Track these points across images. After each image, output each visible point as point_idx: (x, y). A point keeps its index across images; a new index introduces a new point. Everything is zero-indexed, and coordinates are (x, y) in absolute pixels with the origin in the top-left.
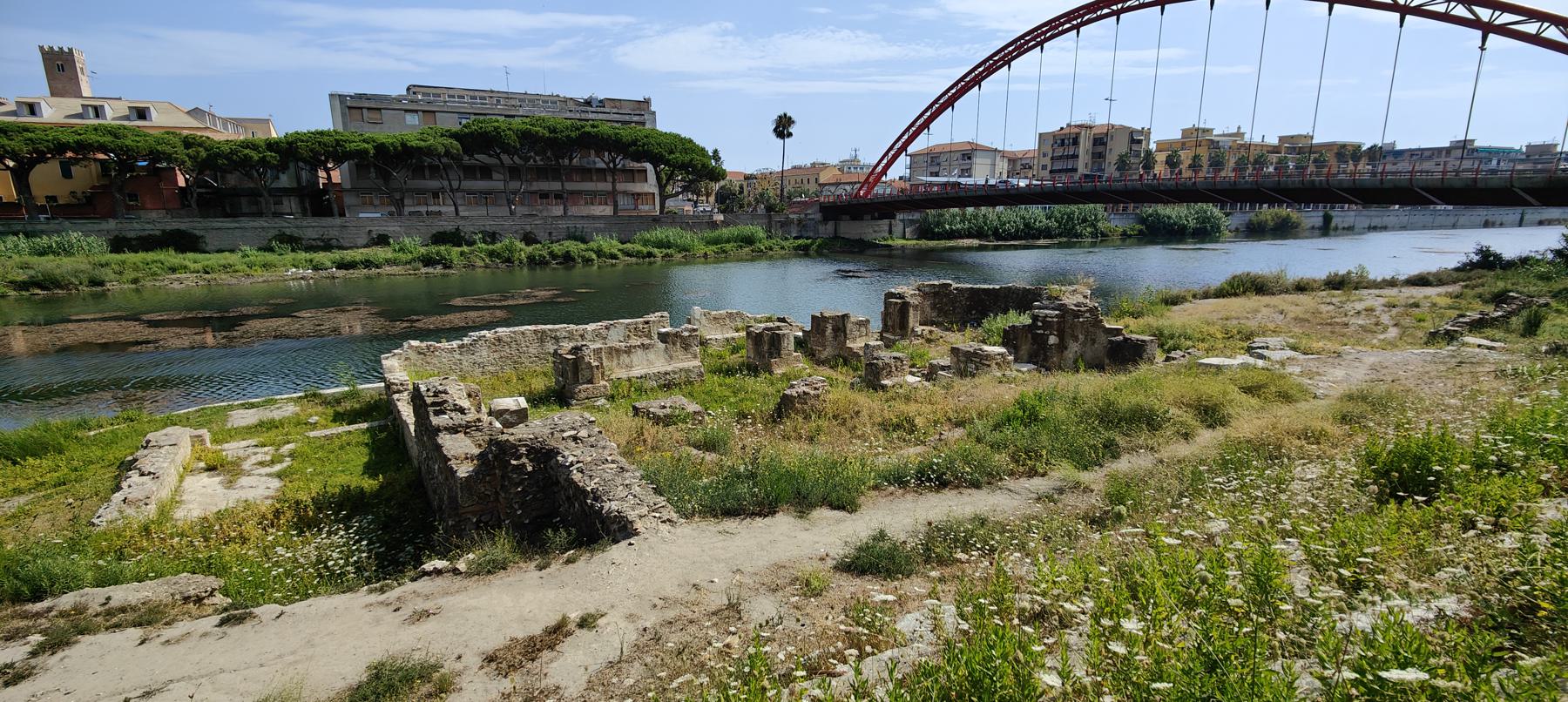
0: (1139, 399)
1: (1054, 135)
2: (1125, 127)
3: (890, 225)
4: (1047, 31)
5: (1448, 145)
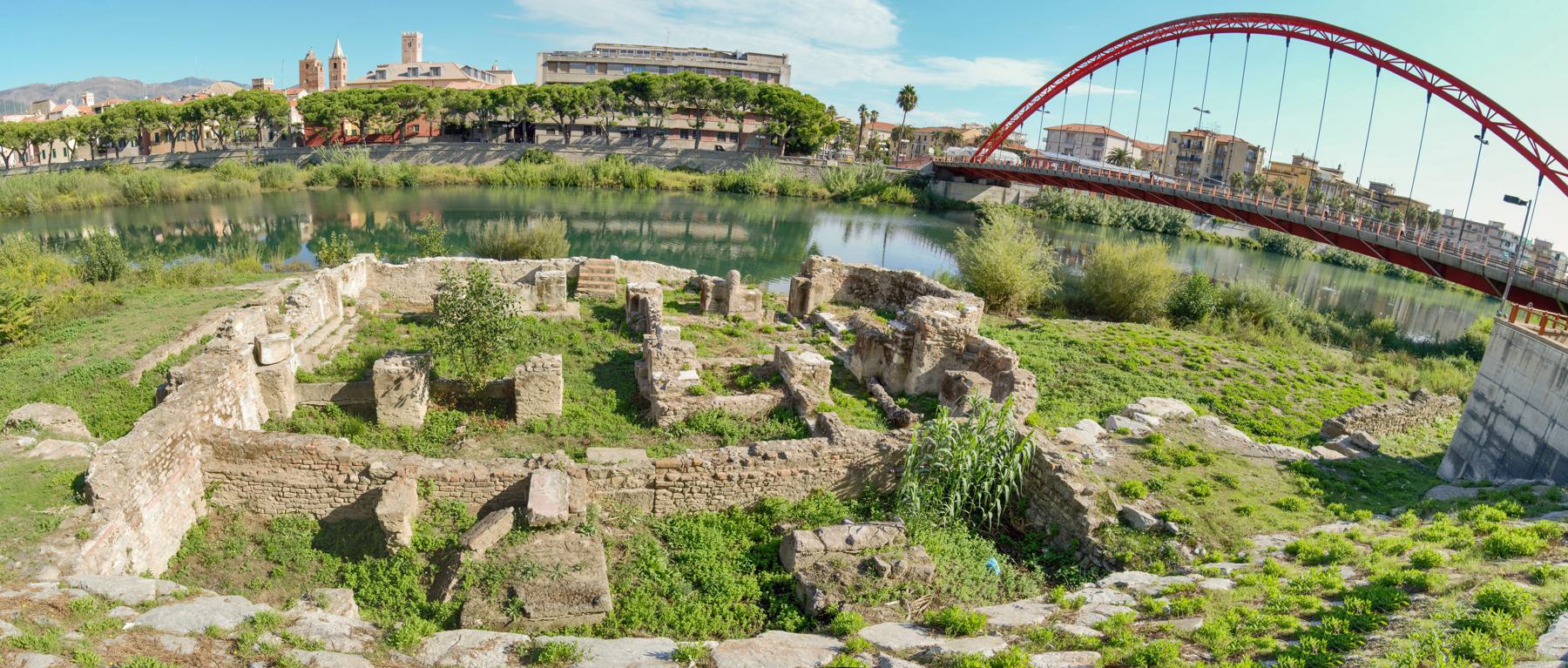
1: (1183, 135)
2: (1243, 142)
3: (1004, 193)
4: (1184, 27)
5: (1487, 223)
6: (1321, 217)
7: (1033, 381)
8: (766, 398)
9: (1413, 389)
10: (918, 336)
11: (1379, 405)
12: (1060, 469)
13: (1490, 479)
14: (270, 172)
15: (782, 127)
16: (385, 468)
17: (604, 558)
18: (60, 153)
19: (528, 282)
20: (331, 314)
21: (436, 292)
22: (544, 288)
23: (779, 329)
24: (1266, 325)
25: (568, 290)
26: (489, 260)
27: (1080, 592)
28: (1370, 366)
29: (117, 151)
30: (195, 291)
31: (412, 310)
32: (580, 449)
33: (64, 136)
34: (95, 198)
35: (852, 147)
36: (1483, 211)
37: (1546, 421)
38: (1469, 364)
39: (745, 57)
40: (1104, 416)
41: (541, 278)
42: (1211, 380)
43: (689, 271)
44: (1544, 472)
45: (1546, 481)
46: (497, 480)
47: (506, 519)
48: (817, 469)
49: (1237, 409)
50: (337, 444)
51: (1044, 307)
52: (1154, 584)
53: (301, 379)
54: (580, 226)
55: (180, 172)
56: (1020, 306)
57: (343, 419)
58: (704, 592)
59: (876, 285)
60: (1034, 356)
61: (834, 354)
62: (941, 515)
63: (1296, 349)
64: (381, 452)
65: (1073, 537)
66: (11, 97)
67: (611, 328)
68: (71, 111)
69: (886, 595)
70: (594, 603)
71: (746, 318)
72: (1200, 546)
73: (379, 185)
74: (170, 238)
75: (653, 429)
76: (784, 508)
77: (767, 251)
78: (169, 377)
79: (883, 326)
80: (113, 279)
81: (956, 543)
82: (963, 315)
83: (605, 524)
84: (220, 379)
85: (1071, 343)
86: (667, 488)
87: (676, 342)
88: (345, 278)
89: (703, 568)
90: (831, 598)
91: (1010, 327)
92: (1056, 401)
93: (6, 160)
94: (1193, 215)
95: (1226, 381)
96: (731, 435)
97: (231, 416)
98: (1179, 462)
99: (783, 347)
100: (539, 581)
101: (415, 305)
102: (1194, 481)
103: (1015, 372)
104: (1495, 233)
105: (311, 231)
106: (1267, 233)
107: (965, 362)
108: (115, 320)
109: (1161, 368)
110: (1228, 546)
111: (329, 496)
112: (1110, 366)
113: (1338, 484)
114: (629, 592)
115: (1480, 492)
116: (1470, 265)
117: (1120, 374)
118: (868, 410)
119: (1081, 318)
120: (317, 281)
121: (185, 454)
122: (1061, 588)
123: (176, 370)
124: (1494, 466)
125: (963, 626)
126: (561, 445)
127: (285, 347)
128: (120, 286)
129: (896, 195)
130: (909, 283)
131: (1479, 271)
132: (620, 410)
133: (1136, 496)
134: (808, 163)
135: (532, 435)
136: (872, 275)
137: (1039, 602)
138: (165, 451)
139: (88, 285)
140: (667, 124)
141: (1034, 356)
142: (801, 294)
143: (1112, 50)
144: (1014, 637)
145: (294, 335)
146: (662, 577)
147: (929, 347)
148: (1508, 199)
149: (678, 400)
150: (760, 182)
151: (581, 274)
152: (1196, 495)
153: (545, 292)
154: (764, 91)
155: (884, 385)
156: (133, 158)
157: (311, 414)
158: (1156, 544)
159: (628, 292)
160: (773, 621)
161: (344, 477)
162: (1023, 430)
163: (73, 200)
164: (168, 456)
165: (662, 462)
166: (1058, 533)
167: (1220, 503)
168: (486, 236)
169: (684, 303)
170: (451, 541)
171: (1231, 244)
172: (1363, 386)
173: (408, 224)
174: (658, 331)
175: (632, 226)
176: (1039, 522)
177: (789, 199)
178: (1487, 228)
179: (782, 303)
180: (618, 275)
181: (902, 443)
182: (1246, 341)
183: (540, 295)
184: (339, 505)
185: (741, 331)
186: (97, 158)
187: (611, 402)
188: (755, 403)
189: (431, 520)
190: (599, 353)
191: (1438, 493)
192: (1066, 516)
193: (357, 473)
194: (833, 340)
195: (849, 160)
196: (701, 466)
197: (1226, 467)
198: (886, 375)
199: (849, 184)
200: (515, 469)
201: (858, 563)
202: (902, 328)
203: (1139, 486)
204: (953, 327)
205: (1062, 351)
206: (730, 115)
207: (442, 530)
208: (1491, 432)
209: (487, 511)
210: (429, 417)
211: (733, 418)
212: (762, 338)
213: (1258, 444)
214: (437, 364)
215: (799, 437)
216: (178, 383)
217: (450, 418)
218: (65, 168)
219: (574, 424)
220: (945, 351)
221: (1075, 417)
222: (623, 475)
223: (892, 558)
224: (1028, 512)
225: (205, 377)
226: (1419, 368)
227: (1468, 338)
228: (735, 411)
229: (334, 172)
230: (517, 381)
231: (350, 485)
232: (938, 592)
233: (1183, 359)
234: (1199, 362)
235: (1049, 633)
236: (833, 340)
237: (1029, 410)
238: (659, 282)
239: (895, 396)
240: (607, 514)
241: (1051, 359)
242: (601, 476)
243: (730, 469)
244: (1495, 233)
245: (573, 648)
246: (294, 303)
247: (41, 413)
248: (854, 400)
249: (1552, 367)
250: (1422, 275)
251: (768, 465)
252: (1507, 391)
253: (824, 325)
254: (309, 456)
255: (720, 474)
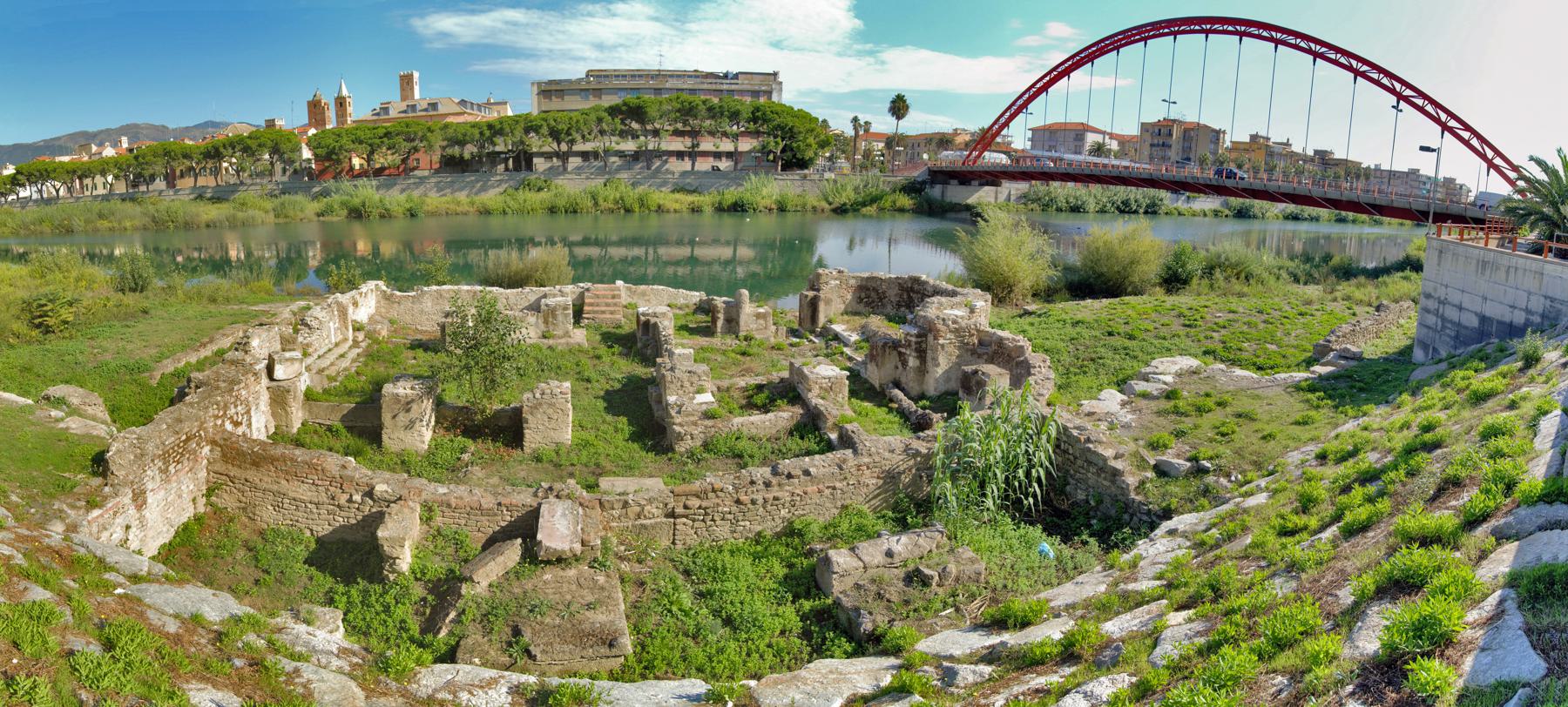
0: (137, 594)
1: (1153, 125)
4: (1151, 30)
6: (1278, 183)
7: (1048, 363)
8: (785, 416)
9: (1375, 304)
10: (930, 338)
11: (1354, 322)
12: (1088, 440)
13: (1453, 352)
14: (282, 204)
15: (777, 143)
16: (390, 490)
17: (621, 595)
18: (100, 186)
19: (533, 310)
20: (341, 337)
21: (444, 320)
22: (549, 316)
23: (791, 345)
24: (1247, 278)
25: (574, 317)
26: (494, 289)
27: (1135, 551)
28: (1338, 294)
29: (148, 185)
30: (212, 308)
31: (419, 337)
32: (591, 480)
33: (103, 173)
34: (128, 224)
35: (847, 159)
36: (1405, 160)
37: (1480, 299)
38: (1414, 275)
39: (736, 76)
40: (1121, 385)
41: (547, 305)
42: (1209, 334)
43: (698, 294)
44: (1489, 335)
45: (1492, 340)
46: (505, 510)
47: (513, 552)
48: (845, 483)
49: (1239, 353)
50: (342, 462)
51: (1047, 294)
52: (1202, 520)
53: (309, 396)
54: (582, 252)
55: (202, 204)
56: (1024, 296)
57: (348, 439)
58: (735, 629)
59: (884, 293)
60: (1047, 339)
61: (849, 364)
62: (982, 511)
63: (1276, 293)
64: (387, 475)
65: (1117, 501)
66: (61, 142)
67: (620, 354)
68: (109, 152)
69: (939, 605)
70: (611, 645)
71: (757, 336)
72: (1234, 473)
73: (386, 216)
74: (189, 259)
75: (670, 455)
76: (815, 528)
77: (774, 267)
78: (189, 380)
79: (896, 332)
80: (141, 291)
81: (1002, 537)
82: (972, 311)
83: (622, 559)
84: (236, 388)
85: (1078, 323)
86: (686, 517)
87: (689, 365)
88: (355, 304)
89: (732, 603)
90: (879, 618)
91: (1020, 316)
92: (1074, 378)
93: (57, 191)
94: (1169, 194)
95: (1223, 332)
96: (751, 457)
97: (241, 424)
98: (1200, 410)
99: (798, 362)
100: (548, 620)
101: (421, 332)
102: (1218, 424)
103: (1029, 358)
104: (1414, 177)
105: (318, 257)
106: (1235, 201)
107: (980, 356)
108: (140, 327)
109: (1164, 331)
110: (1258, 465)
111: (329, 514)
112: (1117, 337)
113: (1339, 391)
114: (650, 634)
115: (1449, 363)
116: (1399, 203)
117: (1128, 343)
118: (891, 417)
119: (1083, 298)
120: (329, 306)
121: (195, 451)
122: (1116, 552)
123: (196, 375)
124: (1452, 343)
125: (1026, 616)
126: (572, 475)
127: (297, 365)
128: (147, 298)
129: (894, 202)
130: (916, 287)
131: (1407, 206)
132: (634, 437)
133: (1166, 446)
134: (805, 177)
135: (540, 465)
136: (878, 283)
137: (1099, 572)
138: (178, 445)
139: (120, 294)
140: (664, 146)
141: (1047, 339)
142: (812, 306)
143: (1063, 67)
144: (1079, 612)
145: (306, 354)
146: (687, 614)
147: (943, 346)
148: (1423, 149)
149: (695, 424)
150: (759, 199)
151: (586, 301)
152: (1223, 435)
153: (550, 319)
154: (758, 109)
155: (902, 390)
156: (162, 191)
157: (316, 432)
158: (1195, 484)
159: (638, 317)
160: (819, 651)
161: (346, 497)
162: (1047, 411)
163: (110, 225)
164: (180, 451)
165: (679, 489)
166: (1102, 502)
167: (1247, 436)
168: (491, 265)
169: (695, 326)
170: (452, 571)
171: (1205, 215)
172: (1337, 311)
173: (412, 253)
174: (671, 354)
175: (637, 251)
176: (1081, 496)
177: (789, 214)
178: (1407, 174)
179: (792, 318)
180: (625, 299)
181: (929, 445)
182: (1233, 294)
183: (546, 322)
184: (338, 524)
185: (754, 350)
186: (131, 191)
187: (622, 430)
188: (773, 422)
189: (431, 547)
190: (608, 379)
191: (1418, 374)
192: (1105, 483)
193: (360, 494)
194: (847, 350)
195: (845, 172)
196: (722, 490)
197: (1244, 405)
198: (903, 380)
199: (847, 196)
200: (524, 498)
201: (902, 575)
202: (915, 331)
203: (1165, 437)
204: (963, 323)
205: (1071, 331)
206: (725, 134)
207: (443, 559)
208: (1444, 319)
209: (494, 542)
210: (434, 443)
211: (752, 438)
212: (775, 355)
213: (1266, 378)
214: (444, 390)
215: (822, 452)
216: (197, 387)
217: (456, 445)
218: (105, 198)
219: (584, 453)
220: (959, 348)
221: (1095, 390)
222: (640, 505)
223: (938, 564)
224: (1068, 488)
225: (223, 385)
226: (1377, 287)
227: (1408, 257)
228: (754, 431)
229: (343, 204)
230: (525, 409)
231: (351, 505)
232: (994, 590)
233: (1182, 321)
234: (1195, 320)
235: (1113, 597)
236: (847, 350)
237: (1049, 391)
238: (669, 306)
239: (916, 400)
240: (622, 548)
241: (1062, 340)
242: (615, 506)
243: (753, 492)
244: (1414, 177)
245: (590, 691)
246: (307, 325)
247: (74, 394)
248: (875, 409)
249: (1474, 262)
250: (1364, 217)
251: (793, 484)
252: (1447, 286)
253: (837, 337)
254: (314, 471)
255: (743, 498)
